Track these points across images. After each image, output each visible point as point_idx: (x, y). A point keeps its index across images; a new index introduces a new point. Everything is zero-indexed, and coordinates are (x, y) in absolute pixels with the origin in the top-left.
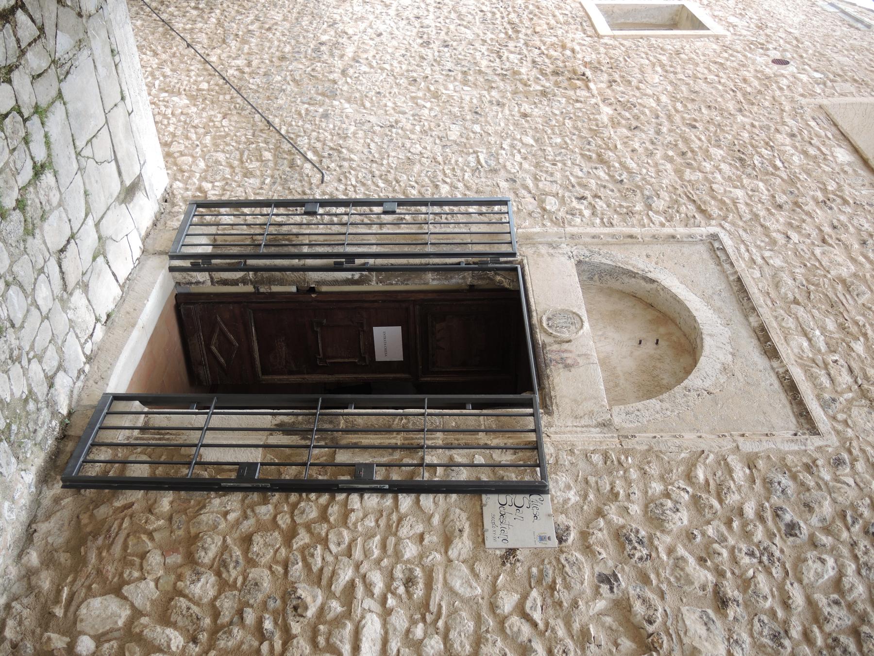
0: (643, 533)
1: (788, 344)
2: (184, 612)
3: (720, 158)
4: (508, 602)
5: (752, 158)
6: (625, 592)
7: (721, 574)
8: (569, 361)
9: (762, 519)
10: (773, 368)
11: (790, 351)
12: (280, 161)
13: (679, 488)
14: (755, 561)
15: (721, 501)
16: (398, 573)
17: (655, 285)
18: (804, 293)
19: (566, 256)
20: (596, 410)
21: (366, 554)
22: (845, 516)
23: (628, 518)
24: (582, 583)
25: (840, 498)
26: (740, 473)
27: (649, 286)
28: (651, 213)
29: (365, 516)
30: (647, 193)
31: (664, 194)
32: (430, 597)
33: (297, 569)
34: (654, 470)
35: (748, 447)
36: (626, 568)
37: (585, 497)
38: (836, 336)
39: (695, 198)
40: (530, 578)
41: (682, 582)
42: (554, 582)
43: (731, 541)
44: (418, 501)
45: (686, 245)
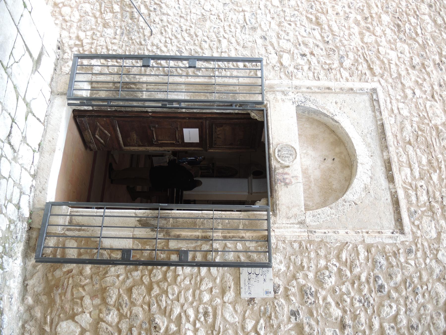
0: (313, 289)
1: (400, 173)
2: (105, 331)
3: (386, 23)
4: (250, 325)
5: (405, 25)
6: (302, 321)
7: (345, 311)
8: (287, 181)
9: (368, 282)
10: (389, 189)
11: (401, 176)
12: (124, 13)
13: (333, 264)
14: (361, 305)
15: (351, 272)
16: (201, 310)
17: (338, 124)
18: (415, 137)
19: (291, 101)
20: (298, 213)
21: (186, 299)
22: (406, 283)
23: (307, 280)
24: (283, 316)
25: (406, 273)
26: (363, 254)
27: (334, 123)
28: (342, 69)
29: (185, 278)
30: (341, 53)
31: (351, 55)
32: (215, 322)
33: (154, 308)
34: (322, 253)
35: (369, 240)
36: (304, 308)
37: (288, 268)
38: (425, 168)
39: (368, 59)
40: (260, 312)
41: (328, 316)
42: (271, 314)
43: (352, 294)
44: (210, 270)
45: (358, 95)
